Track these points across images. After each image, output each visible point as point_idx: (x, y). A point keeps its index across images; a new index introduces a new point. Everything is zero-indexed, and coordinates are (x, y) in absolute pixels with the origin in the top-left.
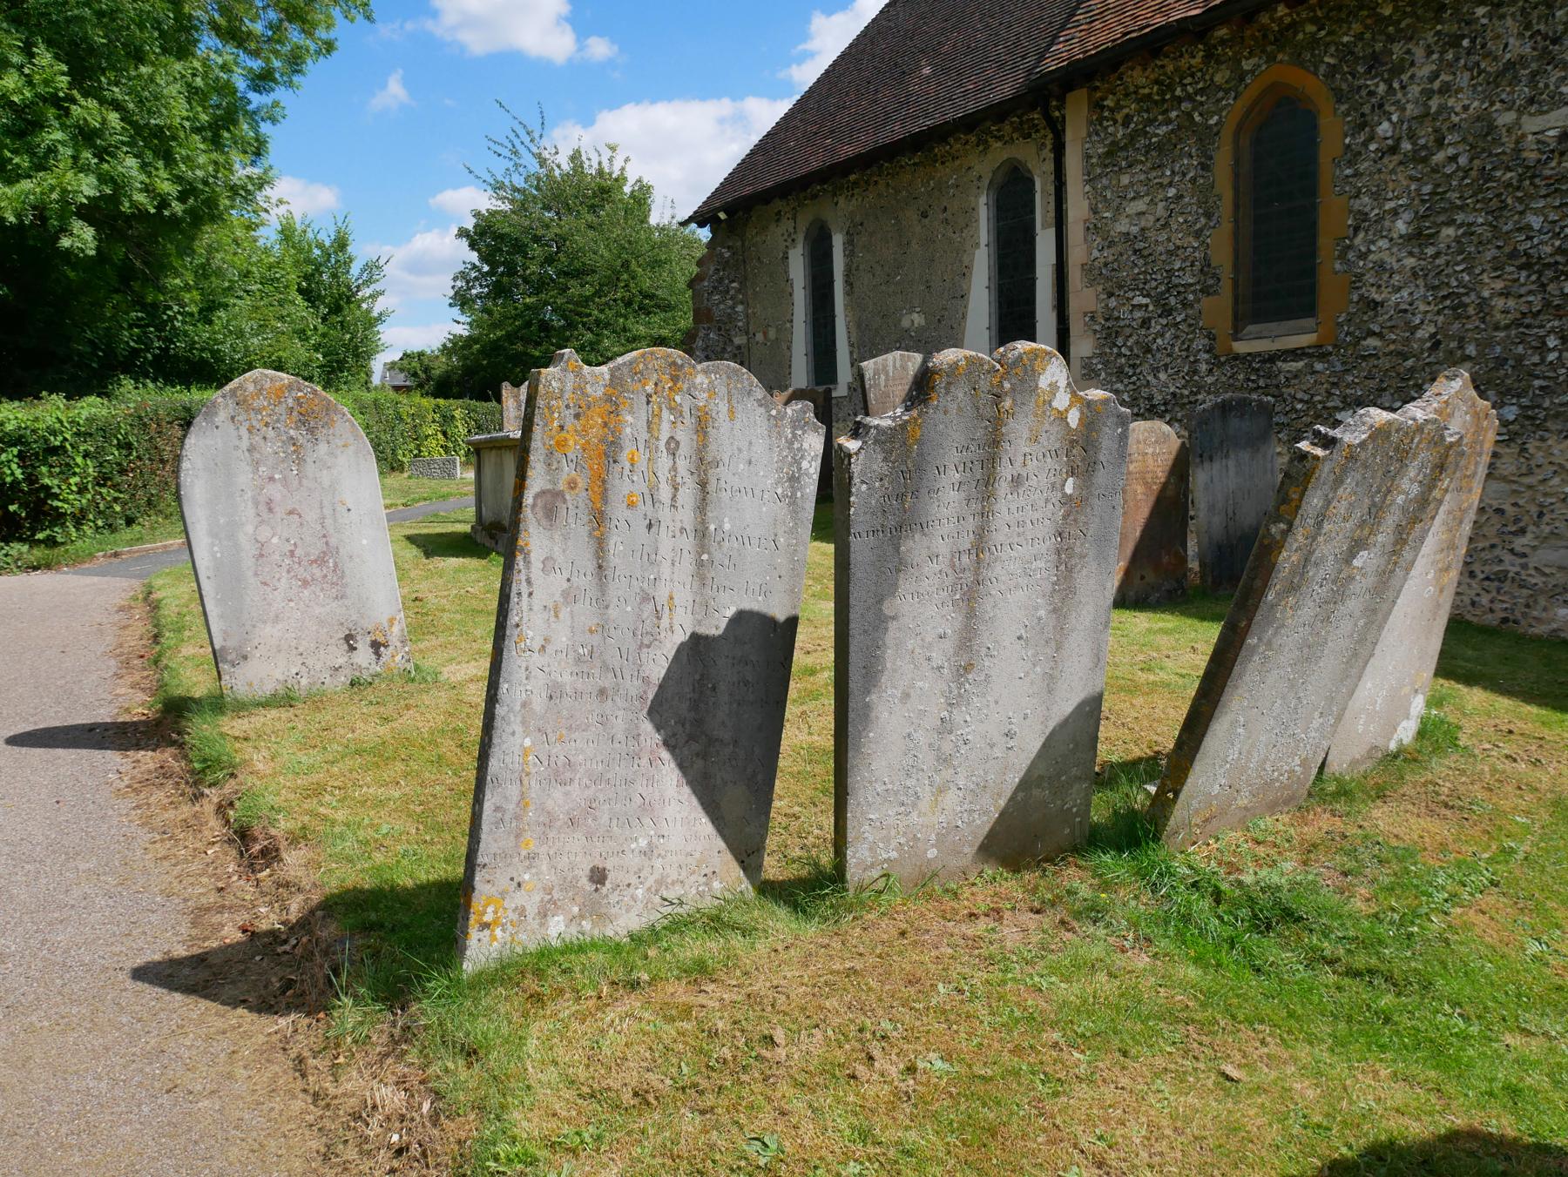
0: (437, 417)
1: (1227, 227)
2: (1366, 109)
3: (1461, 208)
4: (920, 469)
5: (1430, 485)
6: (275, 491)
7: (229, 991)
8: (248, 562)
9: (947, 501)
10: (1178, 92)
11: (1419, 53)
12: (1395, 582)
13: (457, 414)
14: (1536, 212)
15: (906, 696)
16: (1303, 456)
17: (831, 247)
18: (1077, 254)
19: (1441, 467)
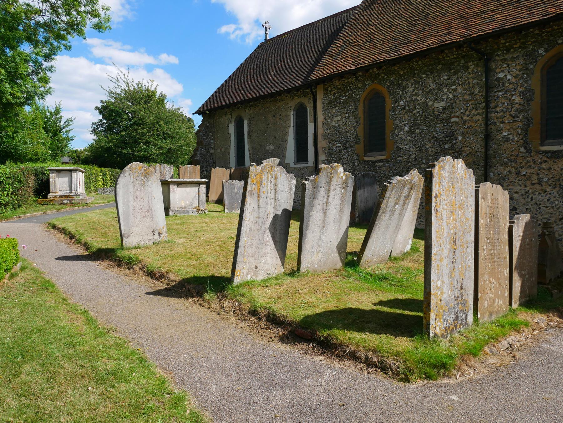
0: (101, 174)
1: (362, 126)
2: (397, 98)
3: (420, 125)
4: (317, 187)
5: (410, 192)
6: (138, 193)
8: (131, 211)
9: (322, 193)
10: (348, 88)
11: (410, 85)
12: (404, 212)
13: (108, 173)
14: (438, 127)
15: (313, 232)
16: (386, 185)
17: (243, 124)
18: (320, 131)
19: (411, 188)
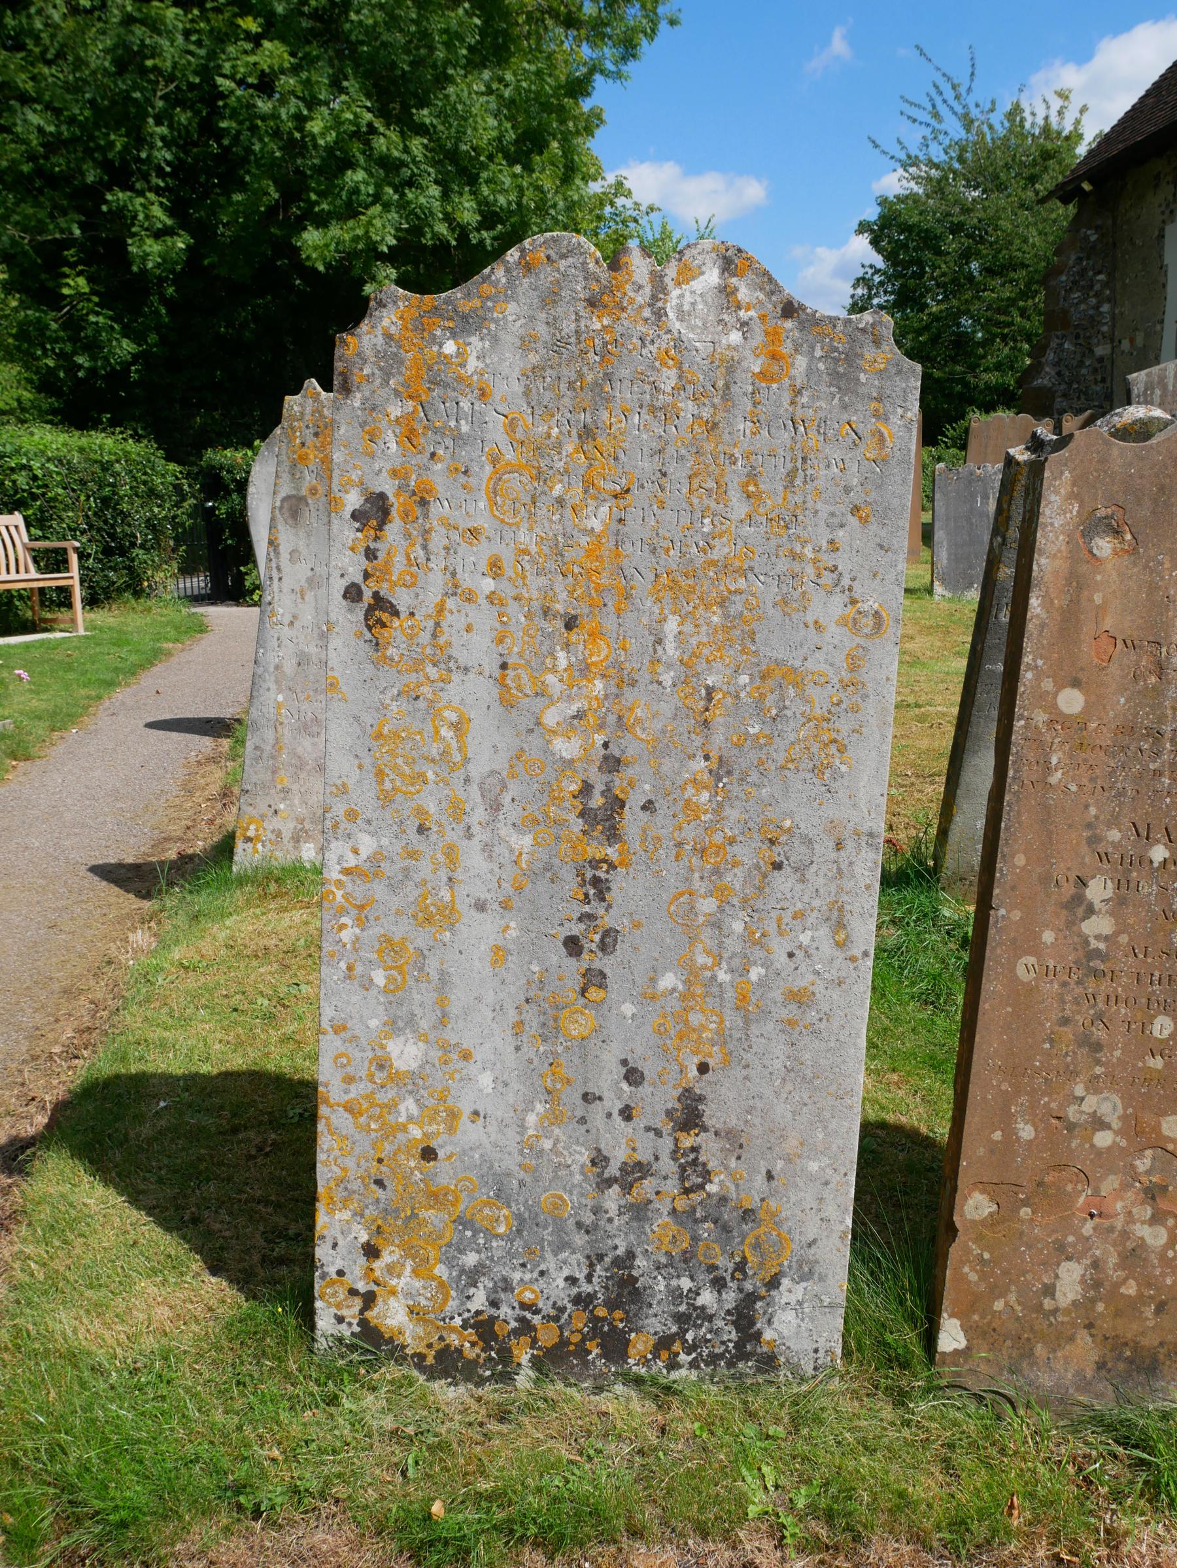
7: (864, 1275)
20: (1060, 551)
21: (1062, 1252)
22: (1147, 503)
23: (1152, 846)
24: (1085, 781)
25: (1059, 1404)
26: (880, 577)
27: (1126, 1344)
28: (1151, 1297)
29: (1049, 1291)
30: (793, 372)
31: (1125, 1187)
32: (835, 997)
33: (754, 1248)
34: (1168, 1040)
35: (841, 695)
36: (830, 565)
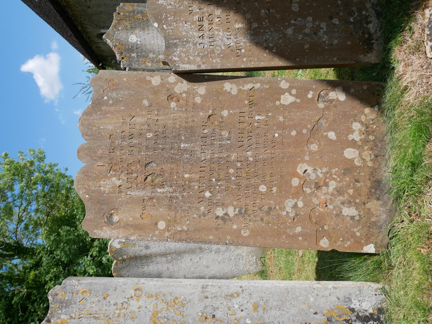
20: (117, 232)
21: (339, 215)
22: (103, 207)
23: (205, 197)
24: (186, 219)
25: (392, 213)
26: (124, 290)
27: (370, 191)
28: (353, 185)
29: (352, 218)
30: (66, 319)
31: (316, 196)
32: (255, 296)
33: (341, 317)
34: (267, 186)
35: (160, 299)
36: (121, 305)
